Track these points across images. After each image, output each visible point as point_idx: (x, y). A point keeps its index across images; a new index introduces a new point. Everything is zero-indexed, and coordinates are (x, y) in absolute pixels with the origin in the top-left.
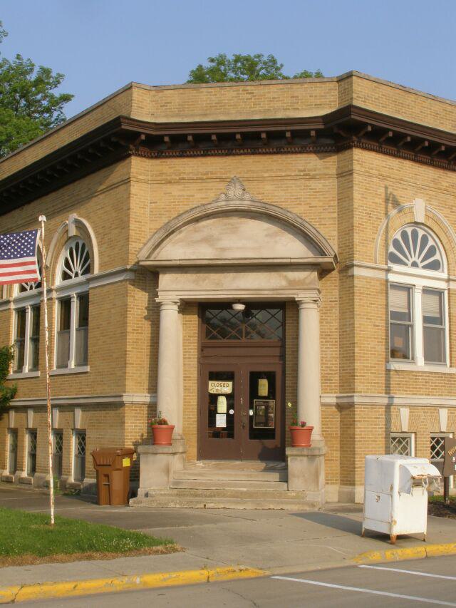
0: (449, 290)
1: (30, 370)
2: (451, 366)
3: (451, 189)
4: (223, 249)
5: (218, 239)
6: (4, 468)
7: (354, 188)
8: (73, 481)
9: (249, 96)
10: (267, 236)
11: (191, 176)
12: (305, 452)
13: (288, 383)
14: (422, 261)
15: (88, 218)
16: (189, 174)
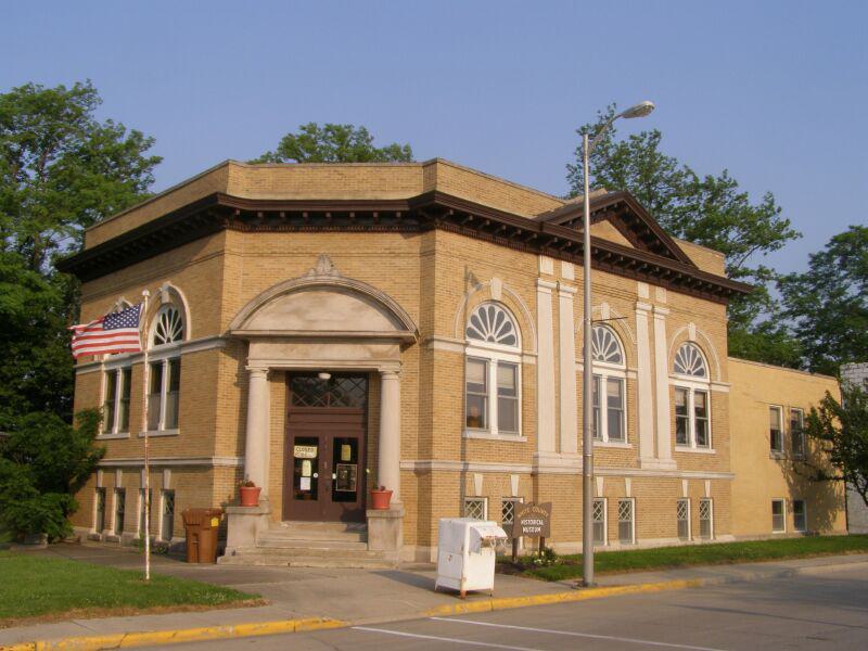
1: (121, 431)
10: (353, 309)
11: (282, 250)
12: (385, 514)
13: (370, 449)
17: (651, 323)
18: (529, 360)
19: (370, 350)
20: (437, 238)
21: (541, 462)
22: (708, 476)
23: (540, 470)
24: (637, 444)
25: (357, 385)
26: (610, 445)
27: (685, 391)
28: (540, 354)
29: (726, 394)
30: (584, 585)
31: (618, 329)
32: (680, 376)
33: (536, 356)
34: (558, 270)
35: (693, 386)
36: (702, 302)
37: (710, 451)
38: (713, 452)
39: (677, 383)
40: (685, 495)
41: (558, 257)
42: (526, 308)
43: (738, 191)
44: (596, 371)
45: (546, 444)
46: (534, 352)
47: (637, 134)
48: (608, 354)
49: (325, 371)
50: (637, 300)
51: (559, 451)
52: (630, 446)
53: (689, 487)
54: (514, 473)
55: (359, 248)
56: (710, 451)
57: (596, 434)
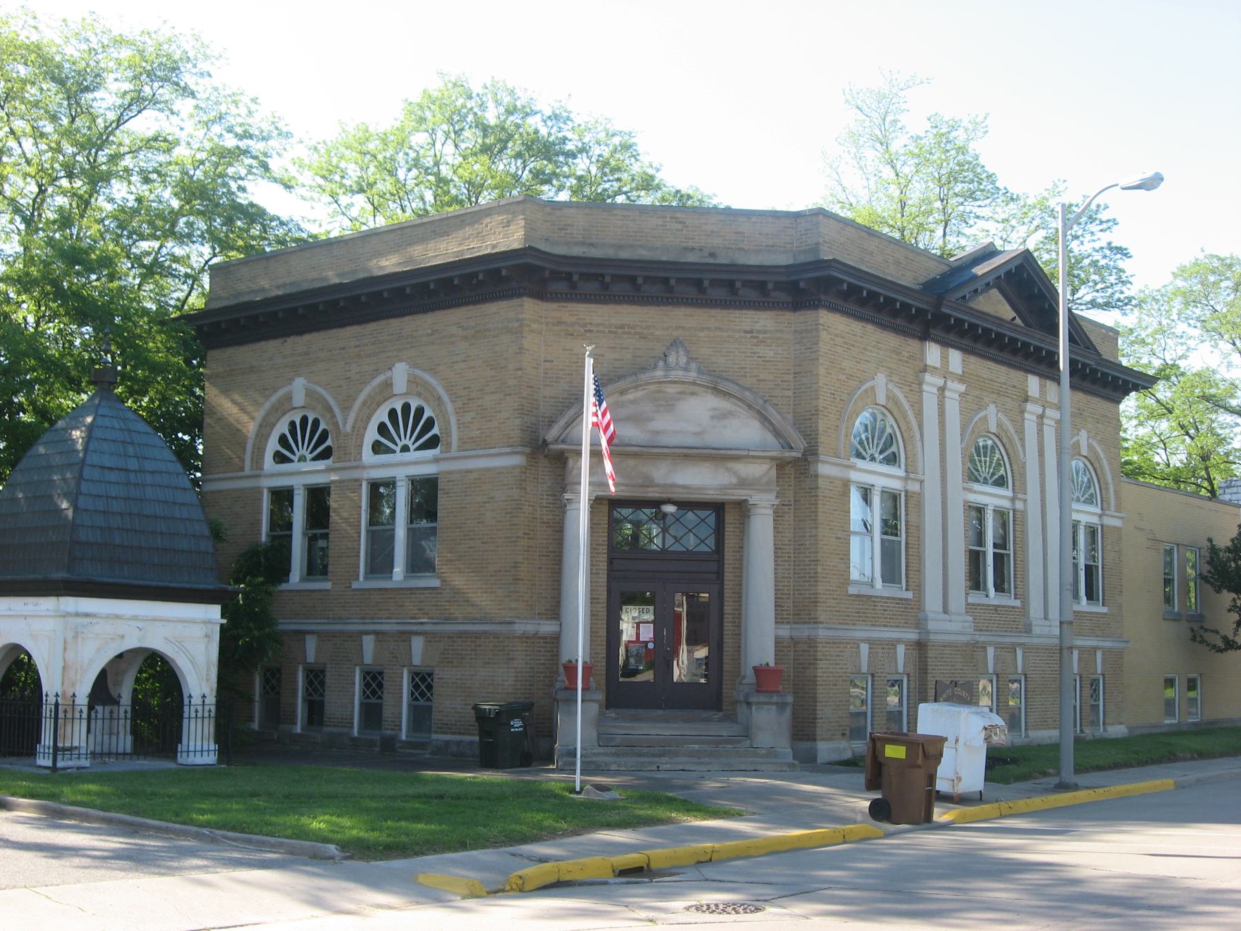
0: (906, 492)
1: (302, 580)
2: (907, 590)
3: (1221, 491)
4: (657, 433)
5: (650, 419)
6: (251, 719)
7: (821, 361)
8: (299, 730)
9: (679, 226)
10: (713, 418)
11: (601, 328)
12: (775, 699)
13: (728, 609)
14: (881, 453)
15: (433, 371)
16: (598, 325)
17: (1040, 426)
18: (914, 487)
19: (735, 473)
20: (821, 321)
21: (931, 626)
22: (1101, 644)
23: (932, 637)
24: (919, 588)
25: (703, 520)
26: (996, 602)
27: (980, 511)
28: (926, 478)
29: (1120, 529)
30: (1063, 787)
31: (1004, 440)
32: (977, 487)
33: (922, 482)
34: (944, 358)
35: (880, 483)
36: (1095, 401)
37: (1100, 609)
38: (1105, 610)
39: (972, 497)
40: (901, 669)
41: (945, 344)
42: (910, 414)
43: (1117, 237)
44: (1075, 516)
45: (932, 602)
46: (920, 477)
47: (1050, 186)
48: (881, 453)
49: (669, 501)
50: (1026, 400)
51: (946, 611)
52: (1018, 603)
53: (996, 658)
54: (367, 633)
55: (709, 329)
56: (1100, 609)
57: (1076, 596)
